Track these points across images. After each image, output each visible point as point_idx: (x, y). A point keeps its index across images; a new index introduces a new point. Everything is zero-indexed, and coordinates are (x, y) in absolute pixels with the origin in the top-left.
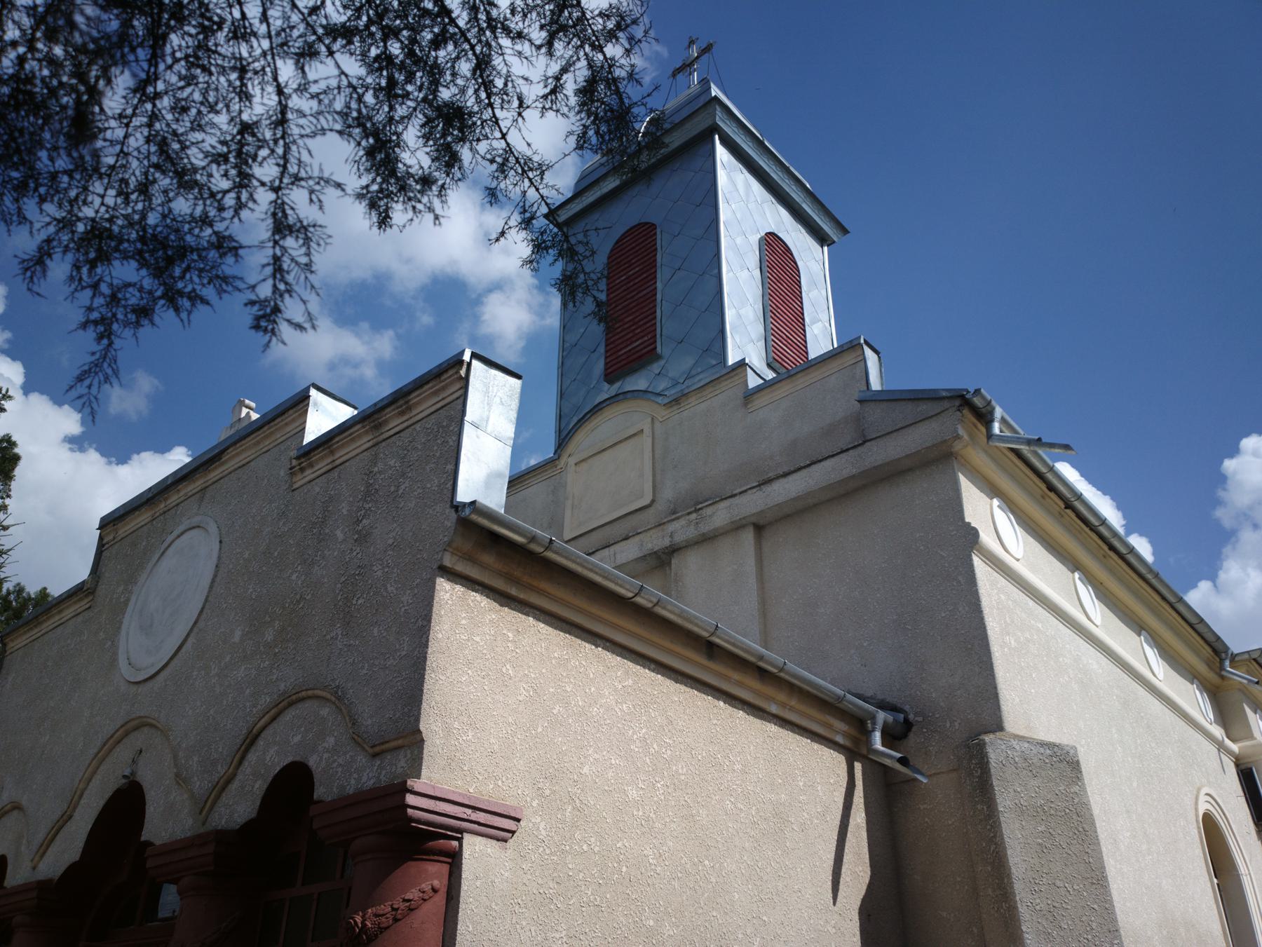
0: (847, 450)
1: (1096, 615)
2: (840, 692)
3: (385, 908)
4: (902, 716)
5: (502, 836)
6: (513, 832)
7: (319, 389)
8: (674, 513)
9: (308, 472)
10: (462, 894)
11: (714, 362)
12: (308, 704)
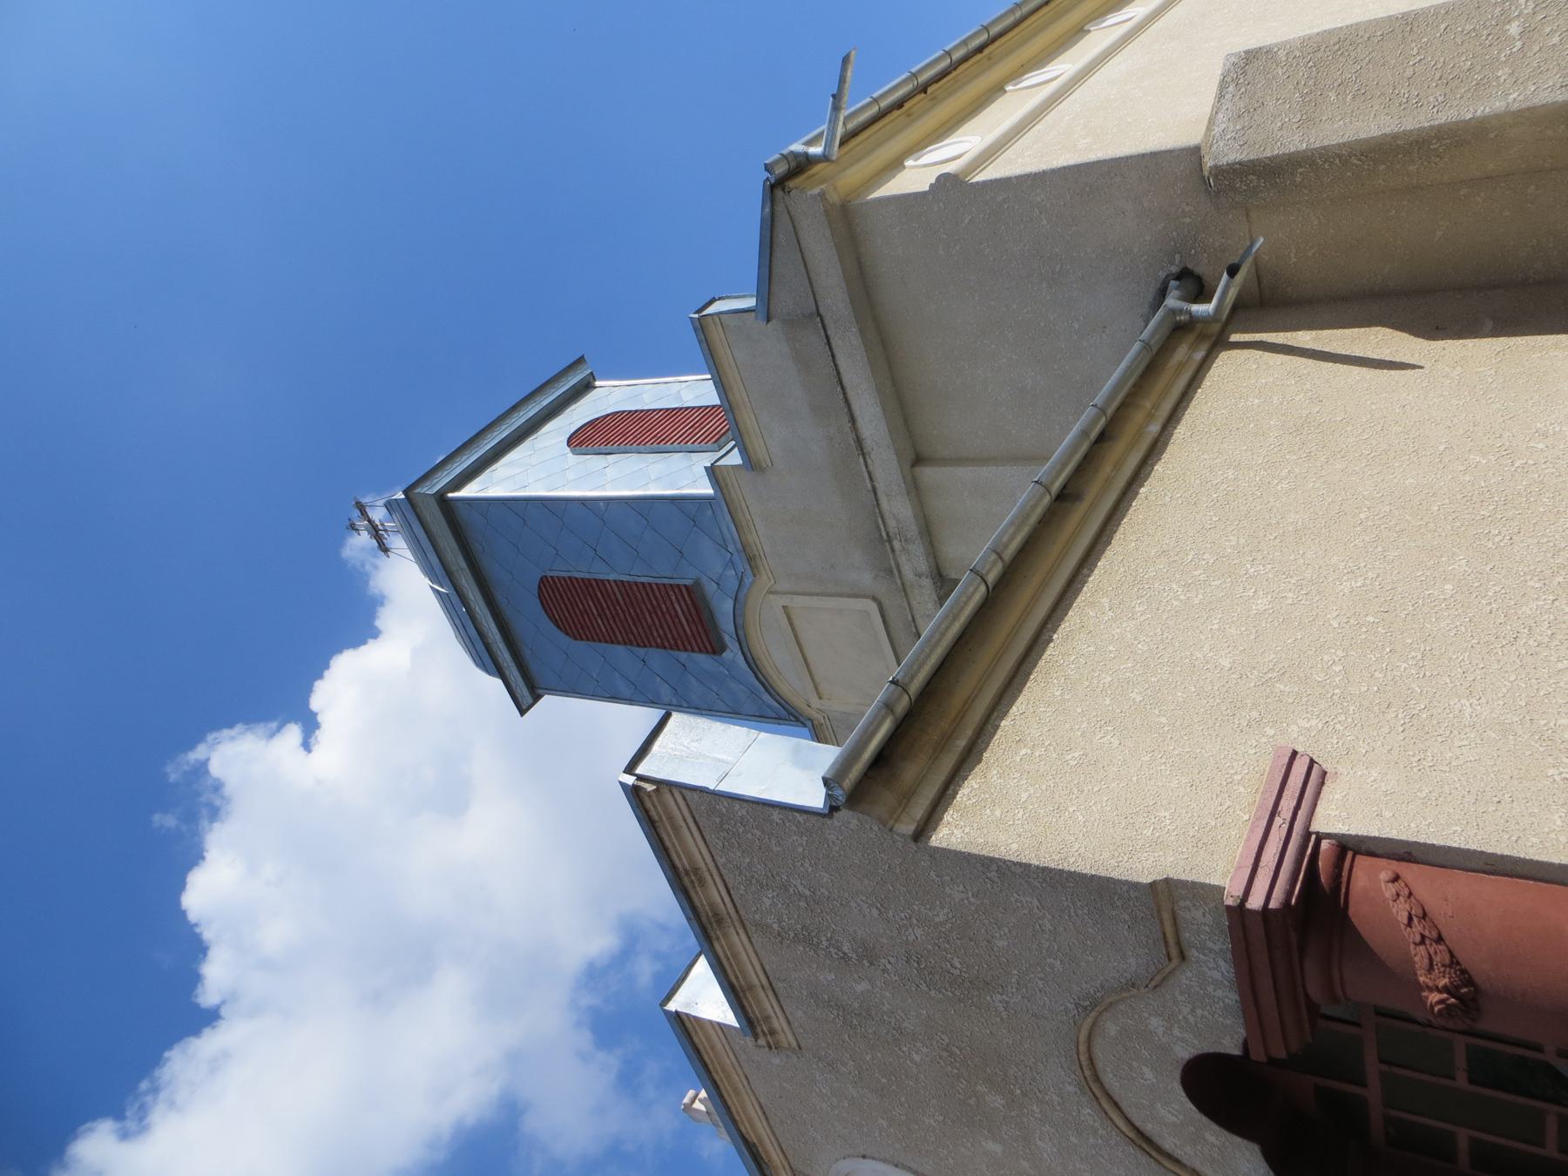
0: (827, 337)
1: (1063, 67)
2: (1137, 346)
3: (1420, 956)
4: (1173, 283)
5: (1316, 778)
6: (1312, 762)
7: (669, 998)
8: (890, 571)
9: (776, 1025)
10: (1404, 837)
11: (710, 512)
12: (1098, 1054)
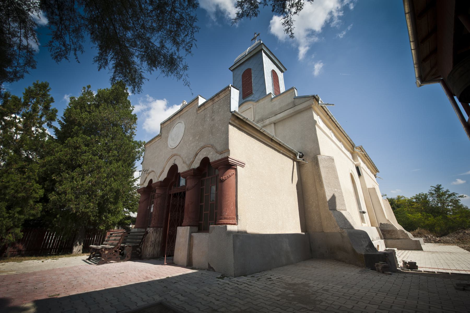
5: (243, 166)
